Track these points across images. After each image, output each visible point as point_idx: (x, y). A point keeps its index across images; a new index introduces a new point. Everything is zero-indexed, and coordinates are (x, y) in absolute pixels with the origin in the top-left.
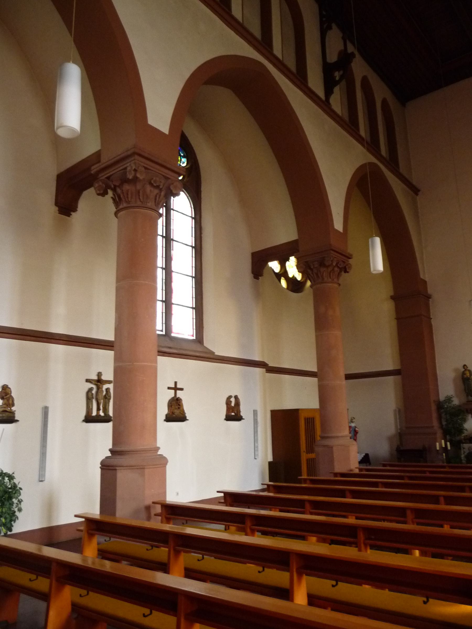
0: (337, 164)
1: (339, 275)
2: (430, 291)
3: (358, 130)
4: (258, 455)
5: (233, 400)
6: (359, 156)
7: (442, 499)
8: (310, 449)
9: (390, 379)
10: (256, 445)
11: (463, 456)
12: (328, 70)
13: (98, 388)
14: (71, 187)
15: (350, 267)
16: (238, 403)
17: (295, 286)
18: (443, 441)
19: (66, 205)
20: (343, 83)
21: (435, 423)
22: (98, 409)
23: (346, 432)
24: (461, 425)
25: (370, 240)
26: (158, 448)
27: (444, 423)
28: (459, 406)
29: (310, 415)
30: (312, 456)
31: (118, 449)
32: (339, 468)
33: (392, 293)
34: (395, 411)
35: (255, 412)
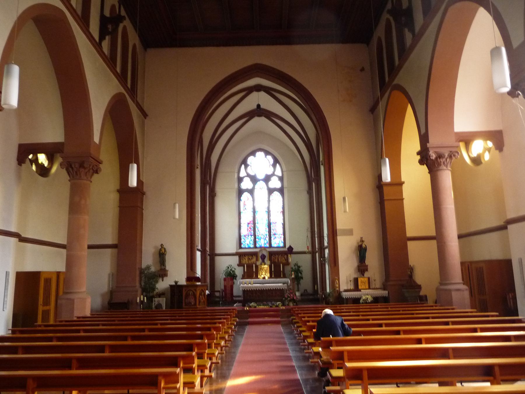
0: (101, 91)
1: (92, 175)
2: (145, 190)
3: (116, 67)
4: (6, 308)
6: (114, 87)
7: (74, 363)
9: (109, 251)
10: (5, 299)
11: (153, 306)
12: (104, 21)
15: (101, 170)
17: (43, 171)
18: (142, 296)
21: (138, 284)
24: (155, 285)
25: (130, 165)
28: (155, 272)
32: (77, 313)
33: (118, 187)
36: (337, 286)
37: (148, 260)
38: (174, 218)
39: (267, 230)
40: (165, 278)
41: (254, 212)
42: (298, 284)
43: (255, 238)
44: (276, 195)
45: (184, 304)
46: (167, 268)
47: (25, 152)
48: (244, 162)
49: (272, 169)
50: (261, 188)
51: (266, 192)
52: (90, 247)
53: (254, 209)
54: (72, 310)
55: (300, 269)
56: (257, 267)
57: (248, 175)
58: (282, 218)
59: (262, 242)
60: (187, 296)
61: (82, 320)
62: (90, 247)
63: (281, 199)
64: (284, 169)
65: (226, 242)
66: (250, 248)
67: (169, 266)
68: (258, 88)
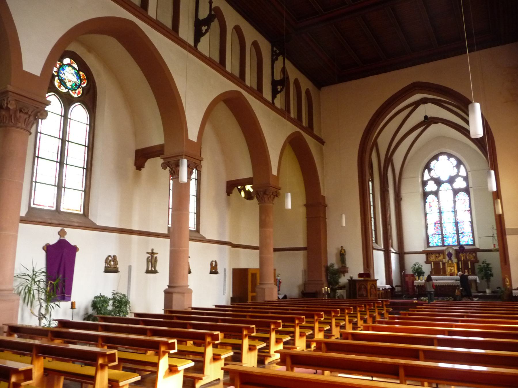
1: (274, 198)
5: (214, 263)
6: (290, 128)
8: (253, 291)
9: (302, 252)
12: (274, 84)
13: (152, 256)
14: (142, 157)
16: (216, 265)
19: (139, 165)
20: (283, 93)
21: (324, 278)
22: (152, 267)
23: (272, 281)
24: (338, 280)
26: (188, 286)
27: (329, 278)
29: (254, 272)
30: (254, 294)
31: (172, 285)
32: (267, 299)
33: (305, 203)
34: (303, 271)
35: (225, 270)
36: (508, 284)
37: (332, 259)
38: (342, 226)
39: (455, 228)
40: (346, 274)
41: (441, 213)
42: (488, 280)
43: (443, 237)
44: (462, 196)
45: (358, 296)
46: (347, 266)
47: (232, 186)
48: (427, 167)
49: (455, 170)
50: (446, 191)
51: (451, 192)
52: (275, 250)
53: (440, 209)
54: (264, 296)
55: (490, 266)
56: (444, 264)
57: (432, 179)
58: (470, 216)
59: (451, 241)
60: (360, 289)
61: (271, 303)
62: (275, 250)
63: (468, 198)
64: (469, 169)
65: (414, 241)
66: (438, 246)
67: (349, 264)
68: (424, 101)
